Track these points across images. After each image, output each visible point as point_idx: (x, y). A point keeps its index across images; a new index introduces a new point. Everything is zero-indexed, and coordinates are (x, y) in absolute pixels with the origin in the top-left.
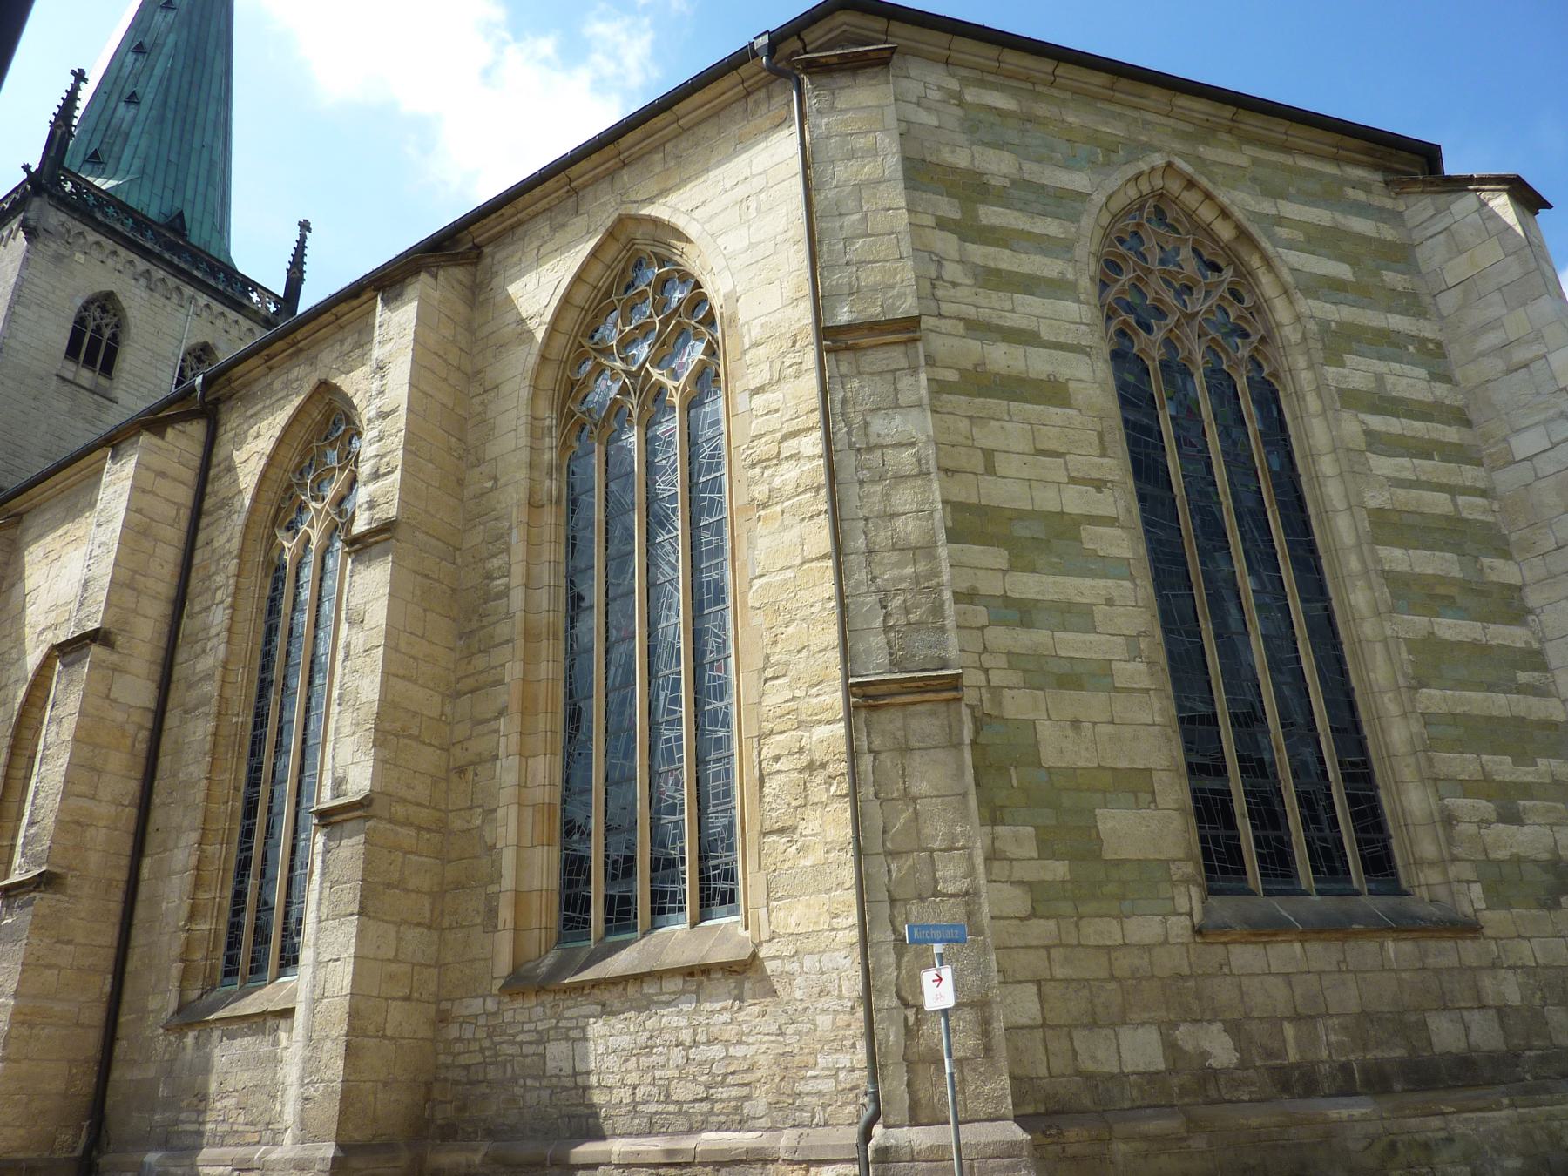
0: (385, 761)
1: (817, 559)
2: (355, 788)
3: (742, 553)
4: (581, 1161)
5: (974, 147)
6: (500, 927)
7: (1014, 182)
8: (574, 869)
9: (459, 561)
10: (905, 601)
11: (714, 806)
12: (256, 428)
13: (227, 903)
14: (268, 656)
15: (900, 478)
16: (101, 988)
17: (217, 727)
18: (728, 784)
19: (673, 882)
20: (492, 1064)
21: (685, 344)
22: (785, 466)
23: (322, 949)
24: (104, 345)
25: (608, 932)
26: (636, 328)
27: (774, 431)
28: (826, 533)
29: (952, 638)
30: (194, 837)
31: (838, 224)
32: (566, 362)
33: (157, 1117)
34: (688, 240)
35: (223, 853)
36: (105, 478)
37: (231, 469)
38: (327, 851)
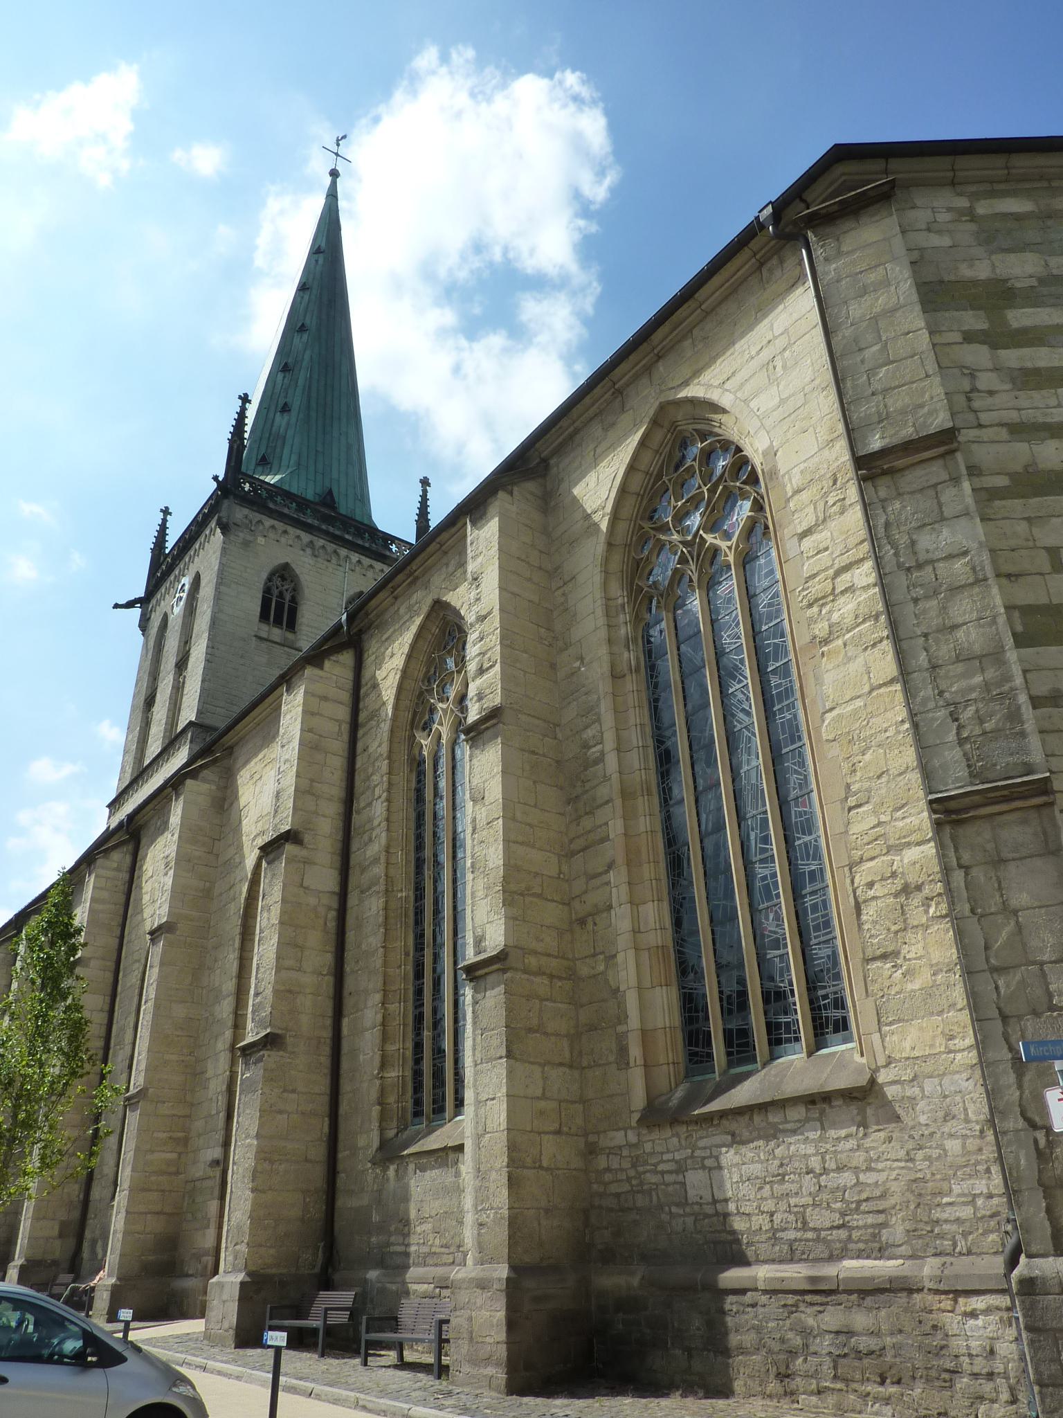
0: (515, 919)
1: (885, 684)
2: (493, 944)
3: (810, 690)
4: (730, 1286)
5: (993, 257)
6: (632, 1063)
7: (1041, 281)
8: (692, 1007)
9: (560, 736)
10: (977, 711)
11: (815, 937)
12: (390, 649)
13: (409, 1053)
14: (419, 837)
15: (955, 590)
16: (322, 1129)
17: (387, 902)
18: (827, 915)
19: (786, 1013)
20: (638, 1192)
21: (734, 505)
22: (842, 600)
23: (480, 1089)
24: (286, 606)
25: (730, 1064)
26: (687, 501)
27: (826, 569)
28: (890, 656)
29: (1034, 742)
30: (378, 997)
31: (859, 359)
32: (630, 545)
33: (374, 1239)
34: (724, 411)
35: (401, 1010)
36: (284, 708)
37: (375, 686)
38: (475, 1003)
